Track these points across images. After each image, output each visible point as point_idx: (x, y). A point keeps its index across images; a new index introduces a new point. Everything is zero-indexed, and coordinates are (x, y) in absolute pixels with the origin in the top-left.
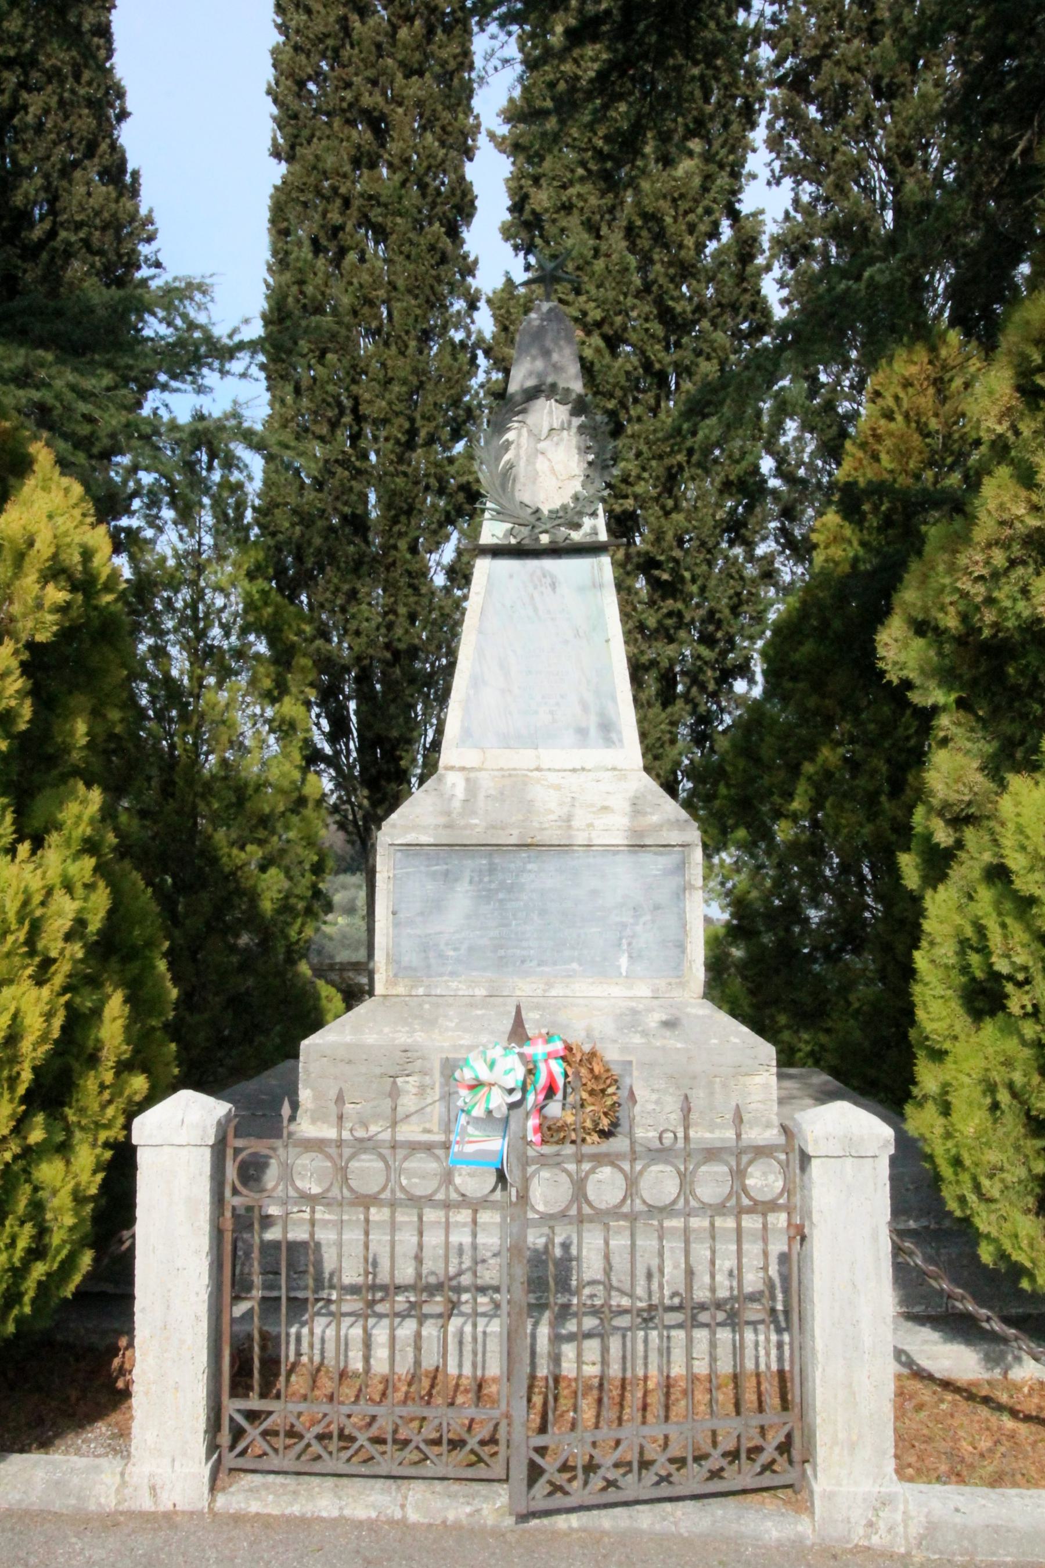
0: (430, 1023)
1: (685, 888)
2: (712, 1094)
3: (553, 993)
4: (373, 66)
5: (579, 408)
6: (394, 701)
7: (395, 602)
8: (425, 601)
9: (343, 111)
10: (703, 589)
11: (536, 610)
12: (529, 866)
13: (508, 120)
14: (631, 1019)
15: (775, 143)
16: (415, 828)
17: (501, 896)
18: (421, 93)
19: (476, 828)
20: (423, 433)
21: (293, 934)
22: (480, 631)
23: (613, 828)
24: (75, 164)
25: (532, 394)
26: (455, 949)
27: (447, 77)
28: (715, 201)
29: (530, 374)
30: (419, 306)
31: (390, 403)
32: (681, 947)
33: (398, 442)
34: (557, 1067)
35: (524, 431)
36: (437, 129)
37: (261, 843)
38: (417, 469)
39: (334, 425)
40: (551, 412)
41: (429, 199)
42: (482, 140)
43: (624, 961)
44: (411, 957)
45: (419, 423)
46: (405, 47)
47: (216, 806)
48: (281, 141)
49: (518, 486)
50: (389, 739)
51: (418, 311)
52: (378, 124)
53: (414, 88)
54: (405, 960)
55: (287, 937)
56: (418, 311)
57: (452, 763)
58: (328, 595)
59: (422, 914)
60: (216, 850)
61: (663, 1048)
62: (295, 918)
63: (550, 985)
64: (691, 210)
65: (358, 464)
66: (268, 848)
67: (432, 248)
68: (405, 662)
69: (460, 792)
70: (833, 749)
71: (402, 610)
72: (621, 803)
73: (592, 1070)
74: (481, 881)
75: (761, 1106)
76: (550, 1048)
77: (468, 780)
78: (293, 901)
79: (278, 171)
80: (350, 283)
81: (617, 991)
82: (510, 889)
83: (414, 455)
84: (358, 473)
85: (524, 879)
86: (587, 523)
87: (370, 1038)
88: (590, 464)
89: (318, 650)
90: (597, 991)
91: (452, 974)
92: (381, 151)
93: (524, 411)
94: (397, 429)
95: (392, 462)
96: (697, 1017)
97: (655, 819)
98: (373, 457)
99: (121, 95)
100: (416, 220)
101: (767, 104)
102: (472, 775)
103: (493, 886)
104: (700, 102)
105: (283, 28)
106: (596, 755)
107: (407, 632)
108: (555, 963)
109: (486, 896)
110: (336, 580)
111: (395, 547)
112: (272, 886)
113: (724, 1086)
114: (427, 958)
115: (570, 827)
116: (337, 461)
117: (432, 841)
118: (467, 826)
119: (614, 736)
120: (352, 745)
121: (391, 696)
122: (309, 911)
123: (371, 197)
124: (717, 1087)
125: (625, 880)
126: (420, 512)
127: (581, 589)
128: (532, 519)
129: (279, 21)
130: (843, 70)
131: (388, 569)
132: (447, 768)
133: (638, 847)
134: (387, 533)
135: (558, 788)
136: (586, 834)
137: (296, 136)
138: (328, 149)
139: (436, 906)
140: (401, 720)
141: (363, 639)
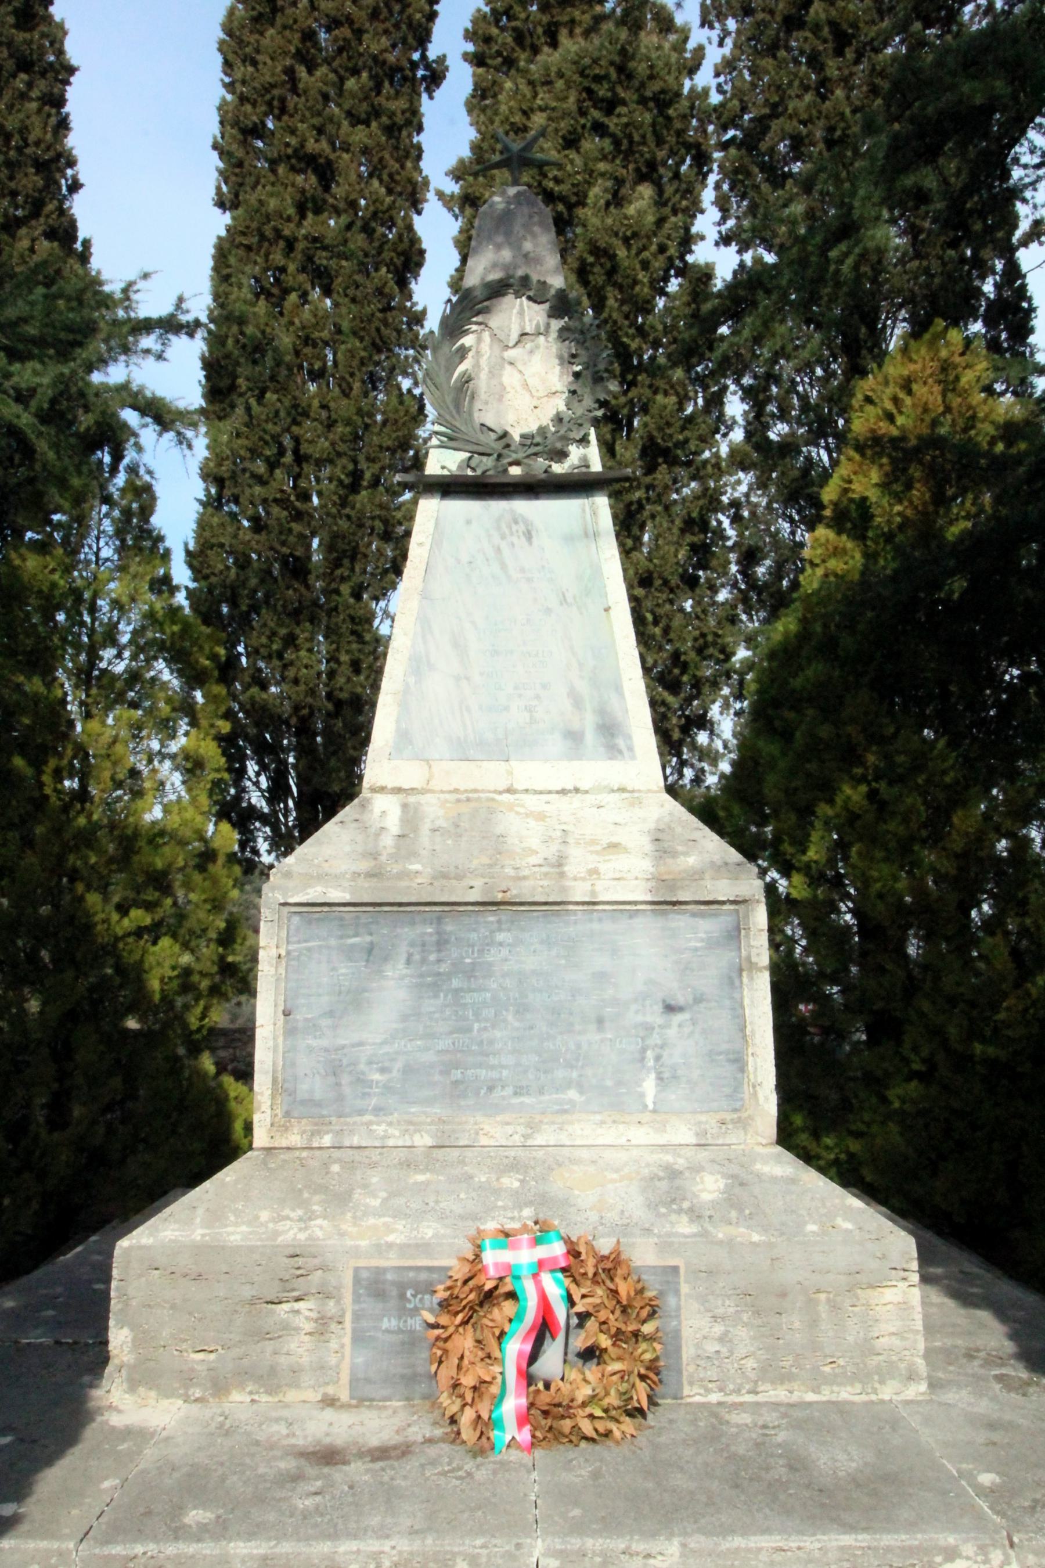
0: (340, 1200)
1: (743, 967)
2: (814, 1323)
3: (539, 1140)
4: (319, 114)
5: (561, 306)
6: (334, 753)
7: (337, 650)
8: (368, 649)
9: (289, 157)
10: (666, 631)
11: (503, 566)
12: (500, 937)
13: (457, 179)
14: (669, 1188)
15: (722, 204)
16: (322, 877)
17: (456, 983)
18: (369, 142)
19: (417, 879)
20: (368, 475)
21: (193, 1022)
22: (425, 595)
23: (629, 877)
24: (19, 222)
25: (497, 290)
26: (383, 1070)
27: (392, 130)
28: (669, 238)
29: (494, 266)
30: (365, 349)
31: (333, 444)
32: (739, 1062)
33: (341, 482)
34: (554, 1287)
35: (486, 336)
36: (385, 177)
37: (149, 906)
38: (362, 512)
39: (272, 465)
40: (521, 313)
41: (376, 244)
42: (431, 196)
43: (649, 1086)
44: (313, 1085)
45: (363, 465)
46: (353, 95)
47: (93, 860)
48: (224, 188)
49: (478, 405)
50: (329, 795)
51: (363, 354)
52: (326, 173)
53: (359, 135)
54: (303, 1088)
55: (185, 1025)
56: (363, 354)
57: (381, 783)
58: (264, 640)
59: (331, 1014)
60: (88, 915)
61: (730, 1244)
62: (197, 1000)
63: (533, 1127)
64: (645, 248)
65: (298, 504)
66: (159, 914)
67: (380, 292)
68: (347, 711)
69: (393, 823)
70: (854, 788)
71: (344, 658)
72: (637, 840)
73: (615, 1292)
74: (424, 961)
75: (896, 1342)
76: (542, 1252)
77: (405, 806)
78: (195, 978)
79: (220, 222)
80: (292, 323)
81: (641, 1135)
82: (470, 972)
83: (359, 498)
84: (298, 516)
85: (493, 956)
86: (575, 453)
87: (235, 1234)
88: (577, 375)
89: (252, 698)
90: (609, 1135)
91: (378, 1110)
92: (327, 196)
93: (486, 311)
94: (341, 469)
95: (334, 504)
96: (774, 1179)
97: (691, 861)
98: (315, 500)
99: (72, 163)
100: (361, 263)
101: (715, 167)
102: (412, 799)
103: (444, 968)
104: (653, 145)
105: (229, 87)
106: (595, 770)
107: (349, 680)
108: (541, 1092)
109: (430, 984)
110: (272, 624)
111: (337, 592)
112: (164, 960)
113: (834, 1307)
114: (338, 1085)
115: (562, 875)
116: (275, 500)
117: (347, 898)
118: (404, 875)
119: (621, 742)
120: (291, 803)
121: (332, 749)
122: (215, 991)
123: (315, 240)
124: (823, 1309)
125: (647, 958)
126: (365, 556)
127: (569, 539)
128: (498, 446)
129: (227, 80)
130: (795, 123)
131: (329, 616)
132: (373, 790)
133: (667, 905)
134: (328, 576)
135: (541, 817)
136: (587, 886)
137: (241, 185)
138: (271, 195)
139: (353, 1001)
140: (342, 774)
141: (302, 687)
